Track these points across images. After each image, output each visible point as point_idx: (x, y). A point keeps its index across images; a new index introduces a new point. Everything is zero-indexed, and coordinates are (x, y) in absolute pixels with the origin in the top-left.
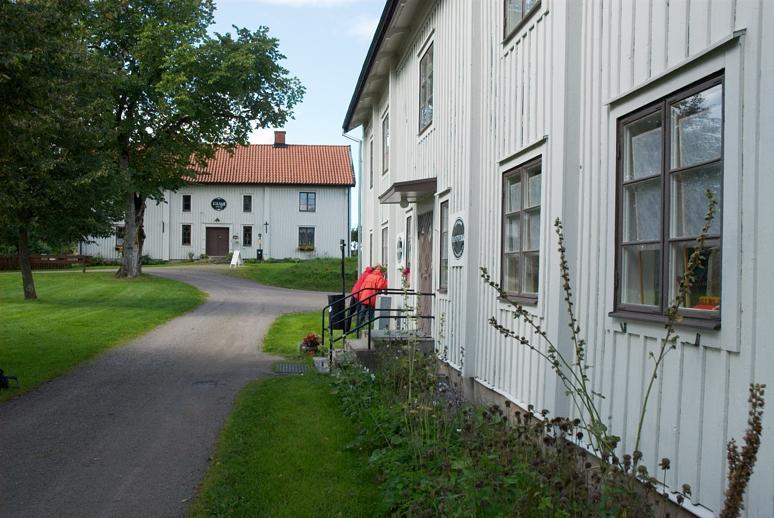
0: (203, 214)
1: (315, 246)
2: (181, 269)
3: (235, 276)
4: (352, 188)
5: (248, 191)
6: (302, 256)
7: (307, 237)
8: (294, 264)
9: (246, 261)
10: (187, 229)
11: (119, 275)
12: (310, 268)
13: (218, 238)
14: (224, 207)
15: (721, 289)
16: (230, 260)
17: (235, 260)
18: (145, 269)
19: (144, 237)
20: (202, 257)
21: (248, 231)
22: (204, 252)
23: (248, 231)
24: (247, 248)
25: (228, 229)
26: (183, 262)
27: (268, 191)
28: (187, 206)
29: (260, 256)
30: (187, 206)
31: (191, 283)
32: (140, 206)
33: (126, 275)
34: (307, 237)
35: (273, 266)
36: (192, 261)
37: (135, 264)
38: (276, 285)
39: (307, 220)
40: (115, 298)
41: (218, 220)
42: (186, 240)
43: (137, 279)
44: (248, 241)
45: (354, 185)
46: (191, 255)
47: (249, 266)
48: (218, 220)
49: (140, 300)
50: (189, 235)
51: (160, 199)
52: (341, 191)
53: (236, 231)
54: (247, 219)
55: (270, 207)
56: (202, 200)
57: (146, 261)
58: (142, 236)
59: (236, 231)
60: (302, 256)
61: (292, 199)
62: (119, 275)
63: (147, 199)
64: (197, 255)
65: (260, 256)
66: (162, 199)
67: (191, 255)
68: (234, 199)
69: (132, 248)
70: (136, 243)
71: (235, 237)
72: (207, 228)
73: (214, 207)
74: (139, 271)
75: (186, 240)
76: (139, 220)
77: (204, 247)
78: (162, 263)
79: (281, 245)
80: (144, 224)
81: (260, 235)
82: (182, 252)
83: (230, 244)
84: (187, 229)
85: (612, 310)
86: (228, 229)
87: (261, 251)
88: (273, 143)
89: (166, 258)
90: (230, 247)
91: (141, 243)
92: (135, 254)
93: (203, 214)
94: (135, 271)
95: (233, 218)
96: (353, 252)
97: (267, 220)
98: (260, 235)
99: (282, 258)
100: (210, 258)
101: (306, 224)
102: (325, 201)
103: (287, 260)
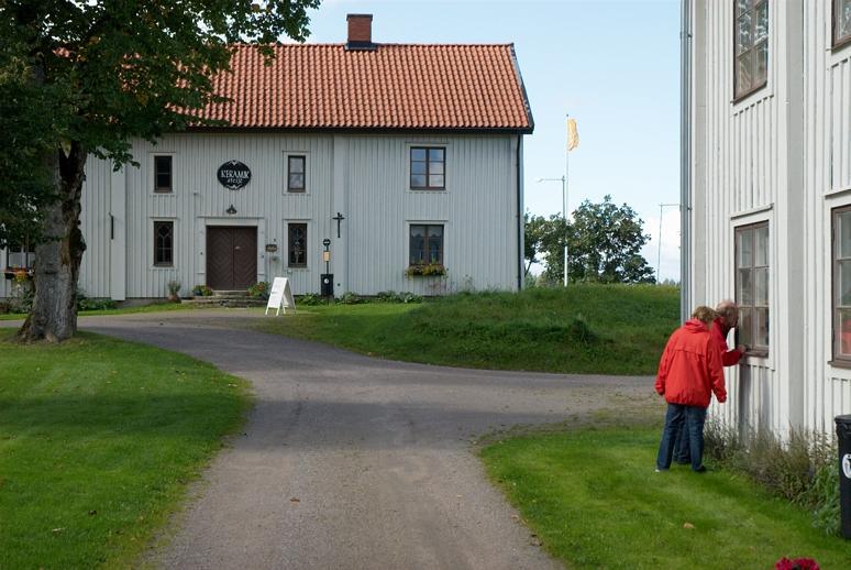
0: (198, 199)
1: (446, 265)
2: (161, 321)
3: (278, 330)
4: (526, 137)
5: (297, 145)
6: (417, 288)
7: (427, 245)
8: (415, 306)
9: (298, 300)
10: (164, 232)
11: (22, 335)
12: (457, 315)
13: (232, 251)
14: (246, 182)
15: (789, 314)
16: (266, 298)
17: (277, 299)
18: (84, 321)
19: (83, 247)
20: (199, 292)
21: (298, 232)
22: (202, 281)
23: (298, 232)
24: (299, 273)
25: (254, 229)
26: (157, 302)
27: (341, 144)
28: (163, 180)
29: (328, 289)
30: (163, 180)
31: (194, 352)
32: (72, 173)
33: (42, 336)
34: (427, 245)
35: (359, 310)
36: (178, 300)
37: (62, 309)
38: (387, 355)
39: (426, 209)
40: (30, 395)
41: (232, 210)
42: (163, 254)
43: (68, 344)
44: (298, 258)
45: (529, 130)
46: (174, 288)
47: (305, 311)
48: (232, 210)
49: (98, 401)
50: (169, 243)
51: (121, 158)
52: (501, 142)
53: (273, 233)
54: (297, 208)
55: (347, 186)
56: (196, 165)
57: (79, 303)
58: (77, 245)
59: (273, 233)
60: (417, 288)
61: (395, 161)
62: (22, 335)
63: (90, 157)
64: (188, 286)
65: (328, 289)
66: (127, 158)
67: (174, 288)
68: (268, 164)
69: (54, 273)
70: (64, 262)
71: (271, 248)
72: (210, 229)
73: (224, 181)
74: (72, 323)
75: (163, 254)
76: (72, 206)
77: (203, 269)
78: (113, 305)
79: (372, 264)
80: (82, 217)
81: (327, 243)
82: (153, 281)
83: (261, 263)
84: (164, 232)
85: (830, 359)
86: (254, 229)
87: (330, 277)
88: (346, 41)
89: (118, 295)
90: (261, 270)
91: (75, 261)
92: (63, 287)
93: (198, 199)
94: (62, 326)
95: (266, 205)
96: (741, 270)
97: (339, 208)
98: (327, 243)
99: (376, 294)
100: (217, 294)
101: (425, 216)
102: (466, 168)
103: (384, 297)
